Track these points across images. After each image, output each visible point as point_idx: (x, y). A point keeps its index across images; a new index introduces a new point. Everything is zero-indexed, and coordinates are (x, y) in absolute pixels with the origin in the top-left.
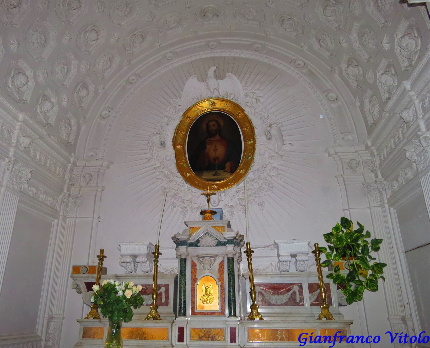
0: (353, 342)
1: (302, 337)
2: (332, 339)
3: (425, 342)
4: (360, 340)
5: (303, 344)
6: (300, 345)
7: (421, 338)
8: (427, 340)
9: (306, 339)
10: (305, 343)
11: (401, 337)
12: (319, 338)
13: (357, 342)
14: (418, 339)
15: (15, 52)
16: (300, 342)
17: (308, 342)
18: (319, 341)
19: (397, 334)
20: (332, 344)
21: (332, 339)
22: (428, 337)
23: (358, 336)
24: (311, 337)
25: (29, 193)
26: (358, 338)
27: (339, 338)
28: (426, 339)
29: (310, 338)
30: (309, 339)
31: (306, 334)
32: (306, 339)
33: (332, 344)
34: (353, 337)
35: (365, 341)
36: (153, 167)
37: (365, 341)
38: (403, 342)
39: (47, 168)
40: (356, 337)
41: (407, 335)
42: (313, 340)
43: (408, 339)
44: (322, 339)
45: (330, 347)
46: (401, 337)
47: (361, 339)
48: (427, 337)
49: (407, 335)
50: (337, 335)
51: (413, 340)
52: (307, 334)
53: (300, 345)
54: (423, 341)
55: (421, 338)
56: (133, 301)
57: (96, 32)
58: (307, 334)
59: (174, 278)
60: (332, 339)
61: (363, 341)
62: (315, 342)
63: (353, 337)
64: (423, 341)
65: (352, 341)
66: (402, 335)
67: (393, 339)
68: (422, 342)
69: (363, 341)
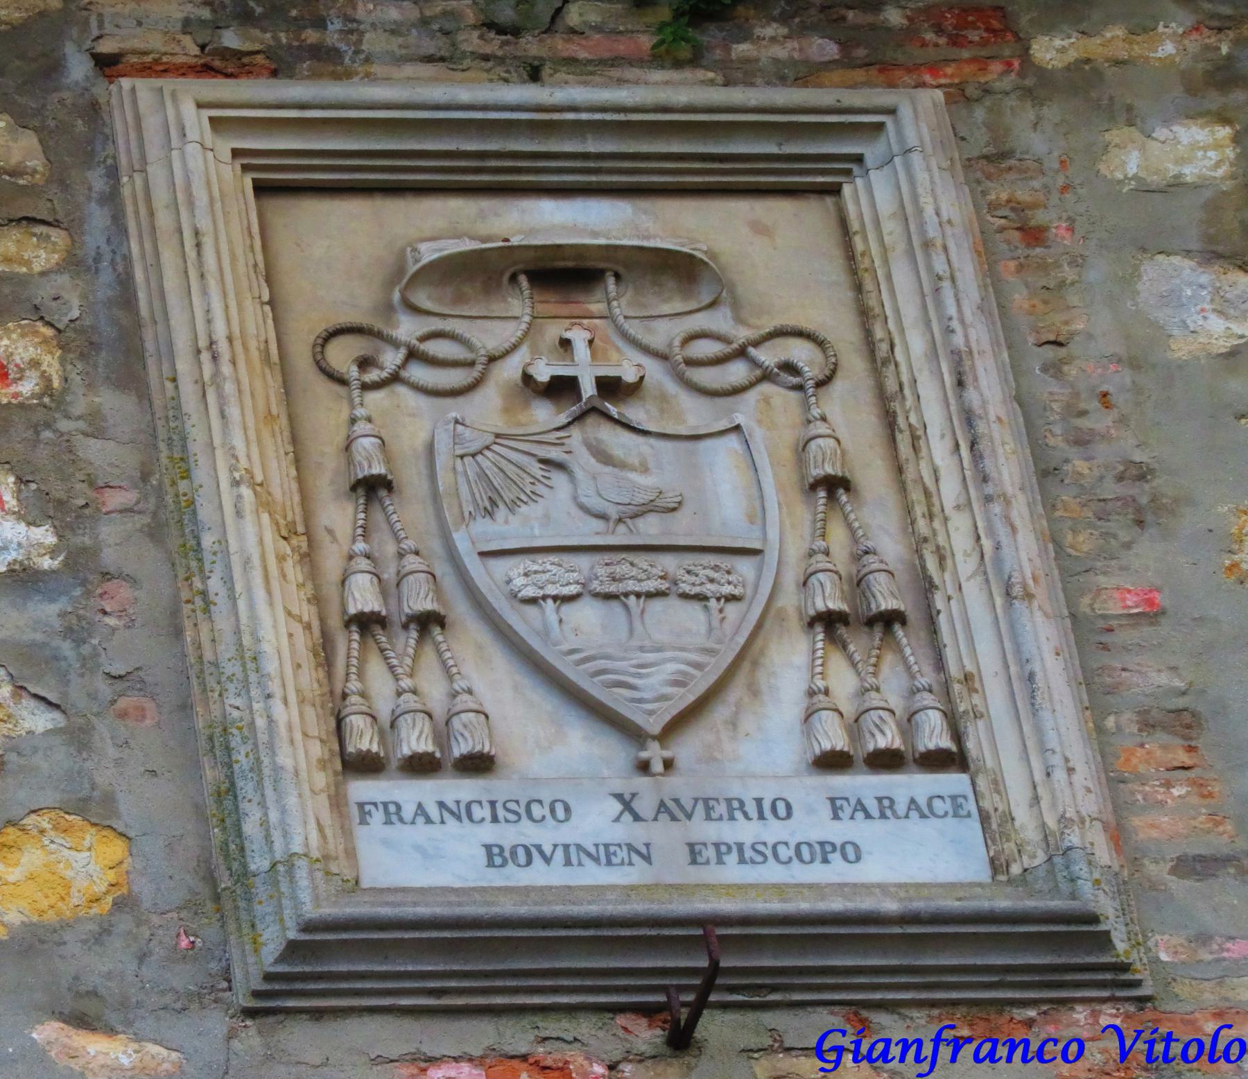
0: (996, 1058)
1: (826, 1046)
3: (1191, 1059)
4: (1034, 1047)
5: (830, 1066)
6: (822, 1070)
7: (1221, 1046)
8: (1075, 1054)
9: (840, 1050)
10: (838, 1062)
11: (1151, 1043)
13: (1009, 1060)
14: (1207, 1046)
18: (992, 1058)
19: (1139, 1033)
20: (925, 1067)
21: (927, 1050)
23: (904, 1041)
24: (858, 1043)
26: (906, 1045)
27: (948, 1045)
28: (1235, 1050)
31: (840, 1034)
33: (925, 1067)
34: (888, 1042)
37: (1220, 1058)
38: (1161, 1059)
39: (153, 988)
40: (897, 1044)
41: (1174, 1037)
43: (1176, 1049)
44: (895, 1051)
45: (920, 1075)
46: (1151, 1043)
47: (914, 1047)
49: (1174, 1037)
50: (943, 1036)
51: (1192, 1052)
53: (822, 1070)
55: (1221, 1046)
56: (983, 23)
57: (49, 332)
59: (844, 472)
60: (927, 1050)
61: (1029, 1058)
63: (888, 1042)
64: (1226, 1055)
66: (1155, 1036)
67: (1127, 1047)
68: (865, 1061)
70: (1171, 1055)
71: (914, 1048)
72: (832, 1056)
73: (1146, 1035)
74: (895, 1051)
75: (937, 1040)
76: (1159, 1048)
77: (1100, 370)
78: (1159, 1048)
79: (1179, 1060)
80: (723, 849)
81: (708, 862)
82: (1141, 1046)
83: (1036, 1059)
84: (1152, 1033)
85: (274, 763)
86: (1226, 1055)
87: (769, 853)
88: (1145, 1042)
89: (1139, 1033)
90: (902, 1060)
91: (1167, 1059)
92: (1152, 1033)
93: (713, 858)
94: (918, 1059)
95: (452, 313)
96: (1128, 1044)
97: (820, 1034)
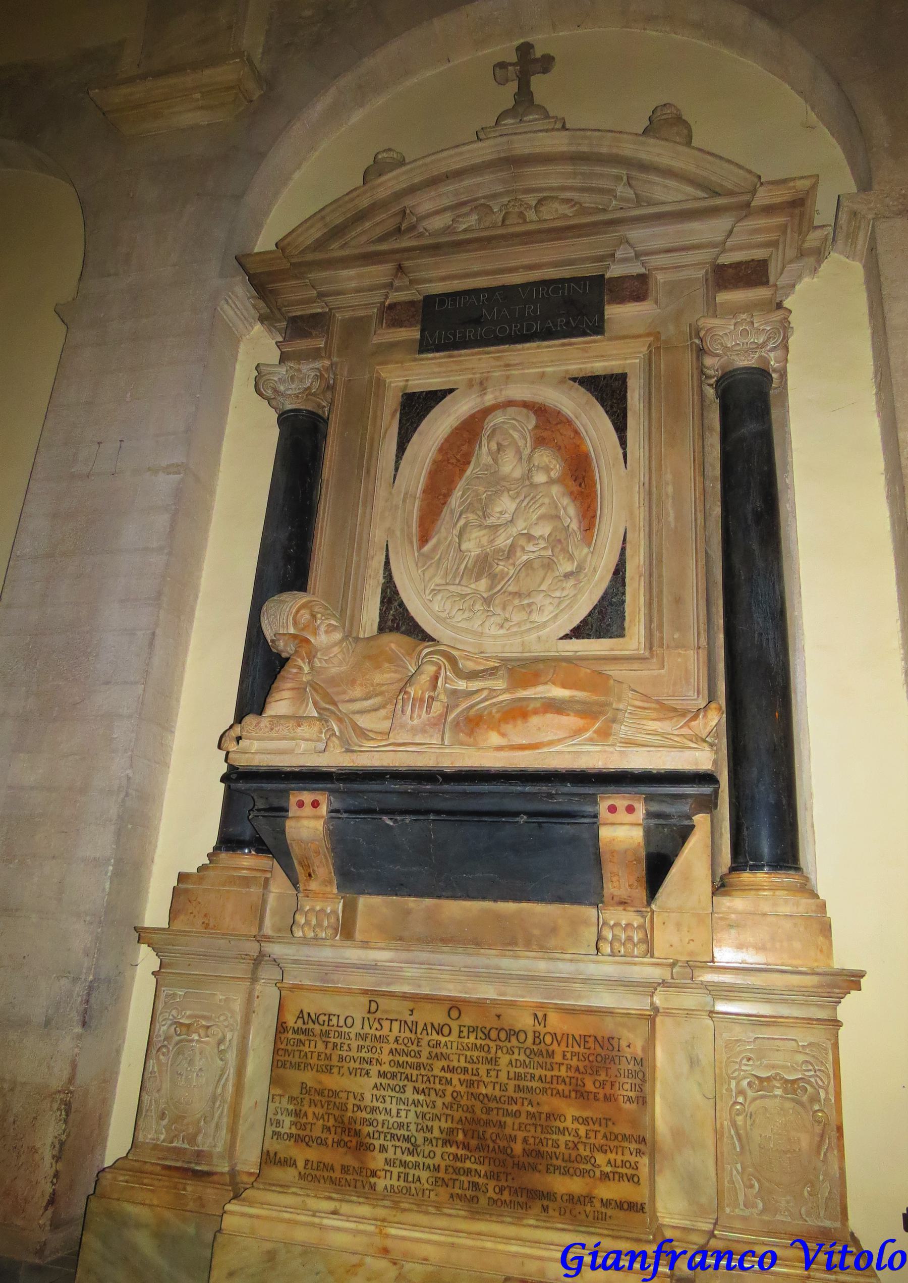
1: (570, 1256)
2: (648, 1261)
6: (566, 1275)
10: (578, 1270)
11: (830, 1254)
12: (614, 1256)
15: (19, 1223)
16: (565, 1266)
17: (586, 1269)
18: (616, 1266)
19: (821, 1246)
21: (650, 1261)
22: (903, 1254)
25: (446, 700)
27: (667, 1256)
29: (827, 1256)
30: (588, 1259)
32: (580, 1259)
34: (619, 1253)
35: (885, 1266)
36: (686, 1012)
37: (885, 1266)
38: (737, 1267)
42: (599, 1261)
45: (644, 1280)
46: (830, 1254)
48: (769, 1254)
52: (583, 1246)
54: (891, 1264)
58: (583, 1246)
60: (650, 1261)
61: (882, 1266)
62: (604, 1266)
65: (702, 1265)
68: (887, 1268)
69: (882, 1266)
70: (846, 1264)
71: (639, 1259)
72: (574, 1265)
73: (826, 1248)
74: (624, 1262)
75: (658, 1252)
76: (836, 1259)
77: (89, 650)
78: (836, 1259)
79: (837, 1269)
80: (574, 1054)
81: (464, 1037)
82: (822, 1257)
83: (887, 1267)
84: (831, 1246)
85: (716, 753)
86: (891, 1264)
87: (509, 1050)
88: (825, 1254)
89: (821, 1246)
90: (630, 1267)
91: (842, 1267)
92: (831, 1246)
93: (570, 1058)
94: (643, 1268)
95: (699, 566)
96: (812, 1255)
97: (563, 1249)
